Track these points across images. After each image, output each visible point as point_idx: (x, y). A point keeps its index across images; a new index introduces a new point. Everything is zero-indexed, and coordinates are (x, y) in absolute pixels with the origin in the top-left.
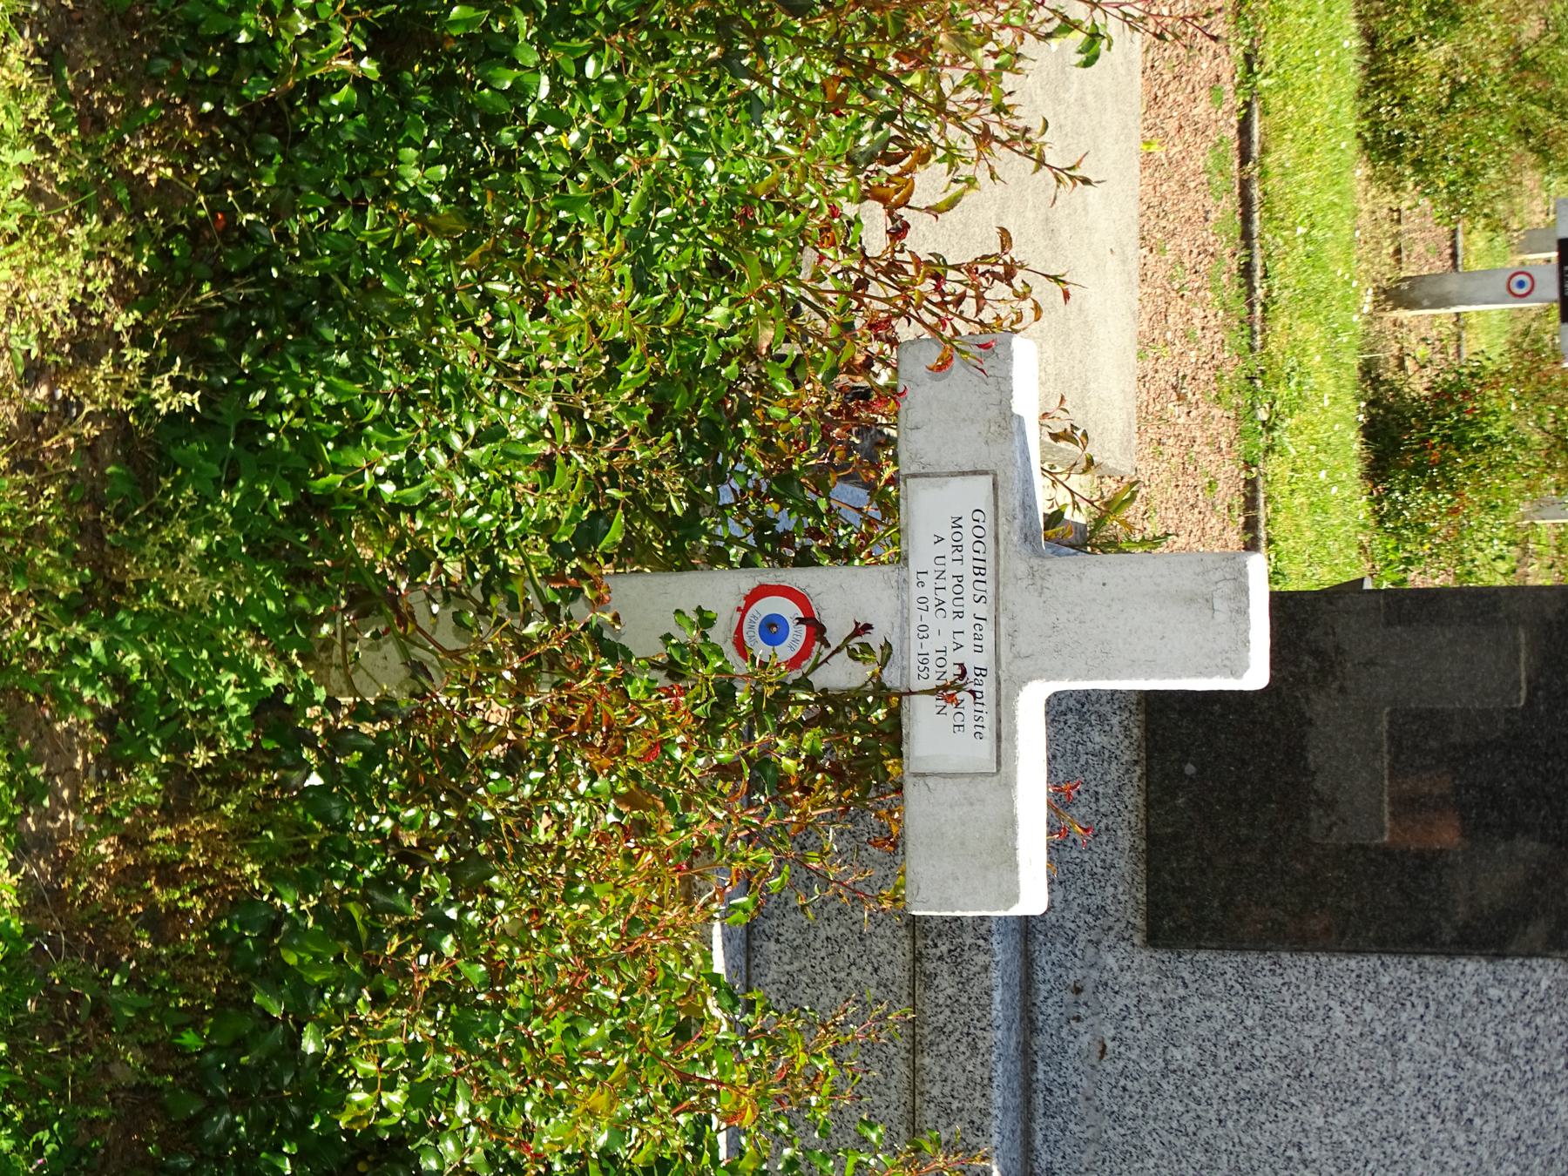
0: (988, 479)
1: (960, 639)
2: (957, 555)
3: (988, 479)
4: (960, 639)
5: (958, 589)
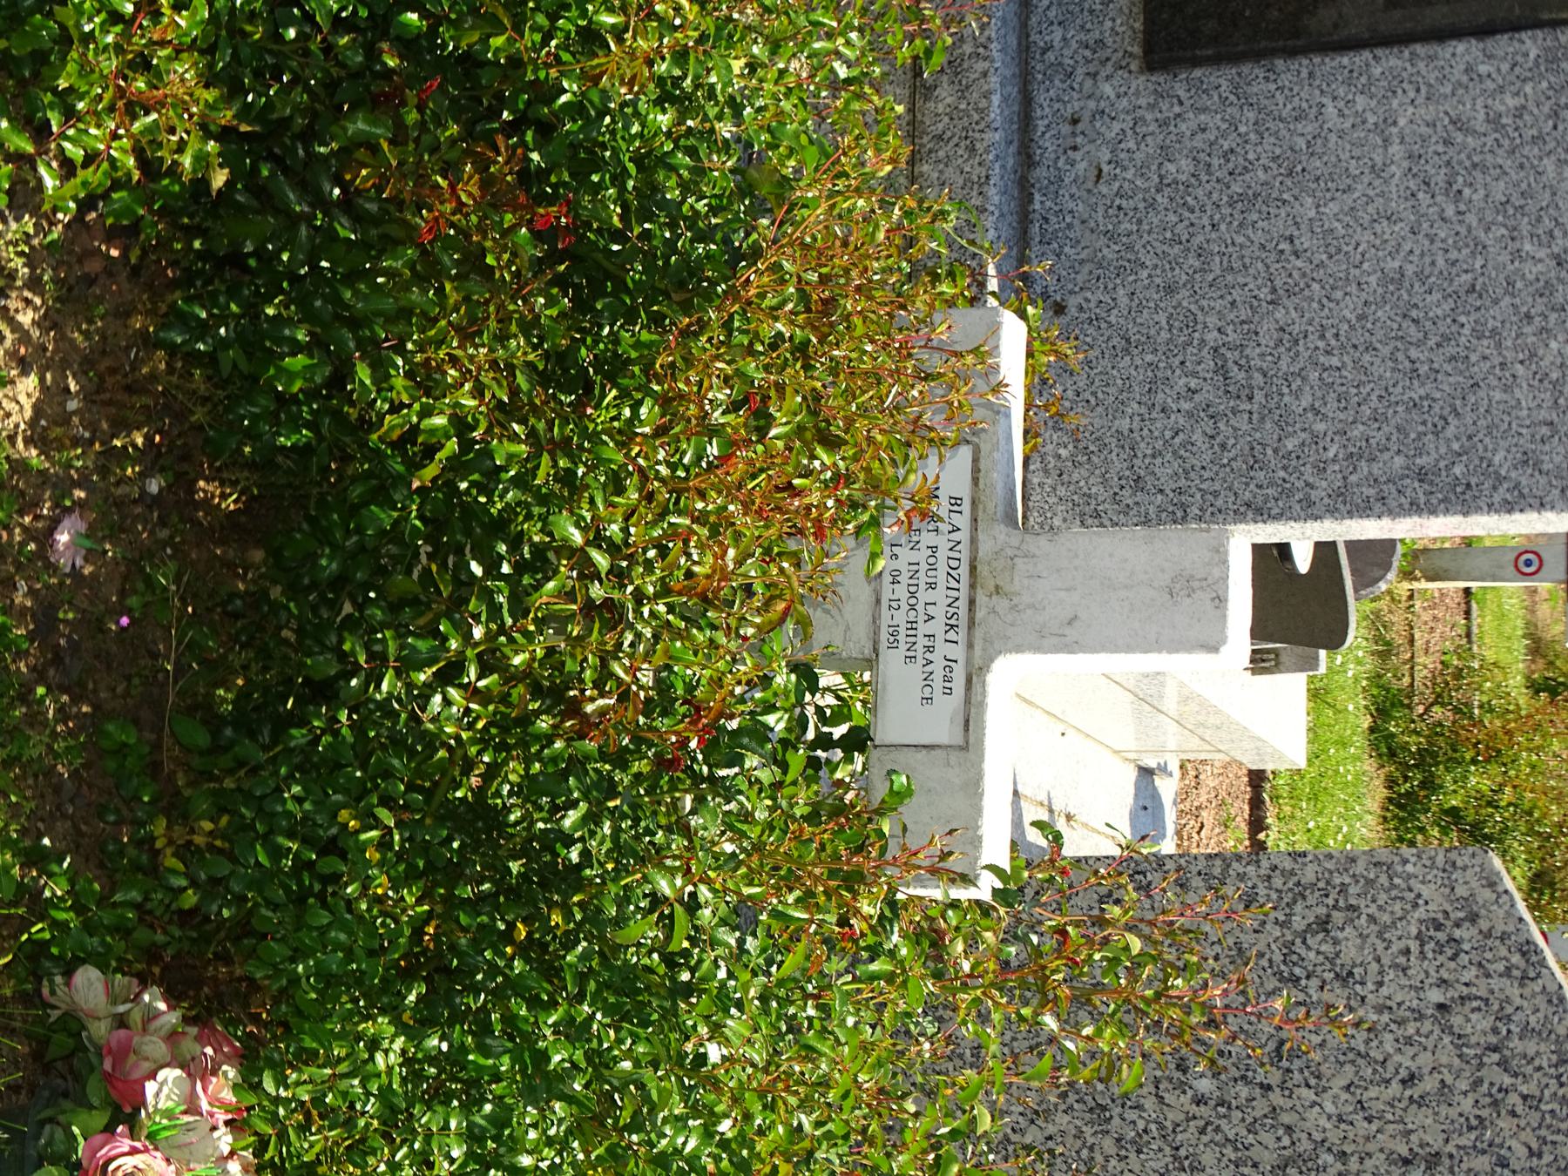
1: (931, 610)
4: (931, 610)
5: (932, 560)
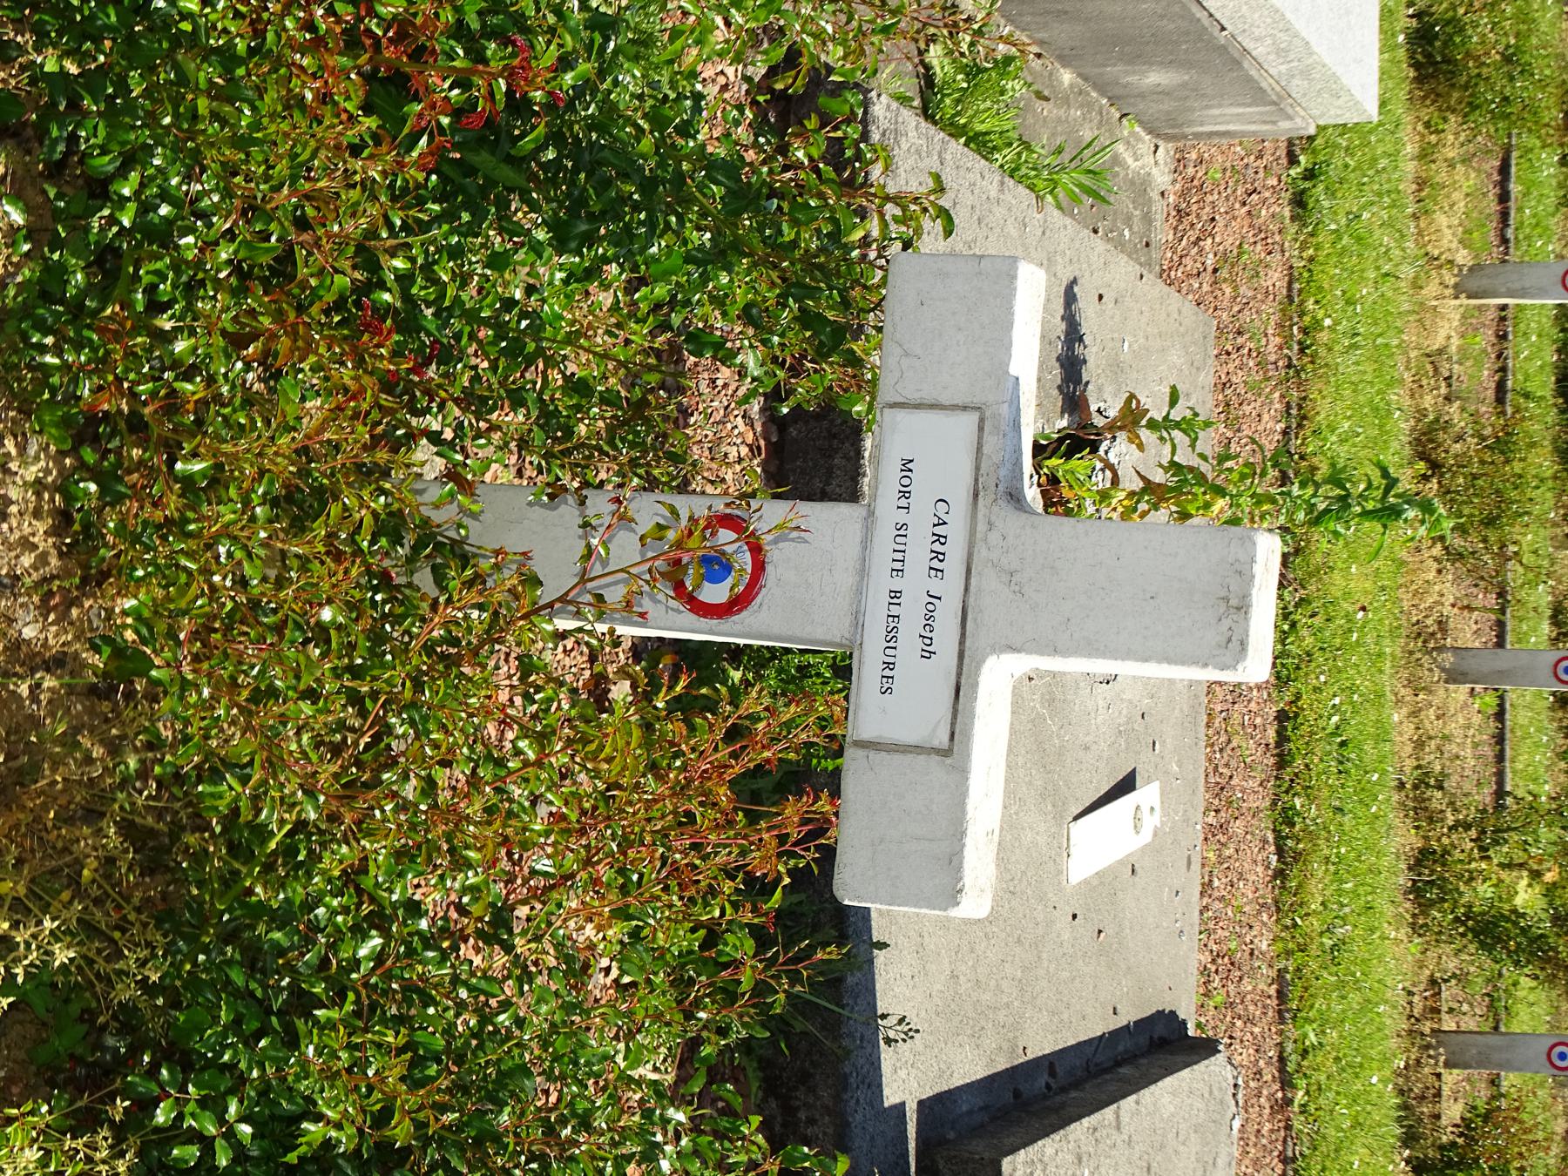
0: (974, 417)
2: (903, 502)
3: (974, 417)
